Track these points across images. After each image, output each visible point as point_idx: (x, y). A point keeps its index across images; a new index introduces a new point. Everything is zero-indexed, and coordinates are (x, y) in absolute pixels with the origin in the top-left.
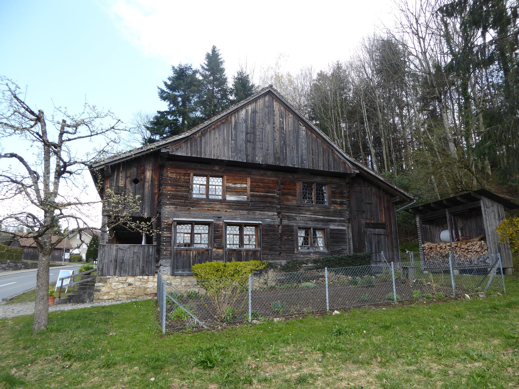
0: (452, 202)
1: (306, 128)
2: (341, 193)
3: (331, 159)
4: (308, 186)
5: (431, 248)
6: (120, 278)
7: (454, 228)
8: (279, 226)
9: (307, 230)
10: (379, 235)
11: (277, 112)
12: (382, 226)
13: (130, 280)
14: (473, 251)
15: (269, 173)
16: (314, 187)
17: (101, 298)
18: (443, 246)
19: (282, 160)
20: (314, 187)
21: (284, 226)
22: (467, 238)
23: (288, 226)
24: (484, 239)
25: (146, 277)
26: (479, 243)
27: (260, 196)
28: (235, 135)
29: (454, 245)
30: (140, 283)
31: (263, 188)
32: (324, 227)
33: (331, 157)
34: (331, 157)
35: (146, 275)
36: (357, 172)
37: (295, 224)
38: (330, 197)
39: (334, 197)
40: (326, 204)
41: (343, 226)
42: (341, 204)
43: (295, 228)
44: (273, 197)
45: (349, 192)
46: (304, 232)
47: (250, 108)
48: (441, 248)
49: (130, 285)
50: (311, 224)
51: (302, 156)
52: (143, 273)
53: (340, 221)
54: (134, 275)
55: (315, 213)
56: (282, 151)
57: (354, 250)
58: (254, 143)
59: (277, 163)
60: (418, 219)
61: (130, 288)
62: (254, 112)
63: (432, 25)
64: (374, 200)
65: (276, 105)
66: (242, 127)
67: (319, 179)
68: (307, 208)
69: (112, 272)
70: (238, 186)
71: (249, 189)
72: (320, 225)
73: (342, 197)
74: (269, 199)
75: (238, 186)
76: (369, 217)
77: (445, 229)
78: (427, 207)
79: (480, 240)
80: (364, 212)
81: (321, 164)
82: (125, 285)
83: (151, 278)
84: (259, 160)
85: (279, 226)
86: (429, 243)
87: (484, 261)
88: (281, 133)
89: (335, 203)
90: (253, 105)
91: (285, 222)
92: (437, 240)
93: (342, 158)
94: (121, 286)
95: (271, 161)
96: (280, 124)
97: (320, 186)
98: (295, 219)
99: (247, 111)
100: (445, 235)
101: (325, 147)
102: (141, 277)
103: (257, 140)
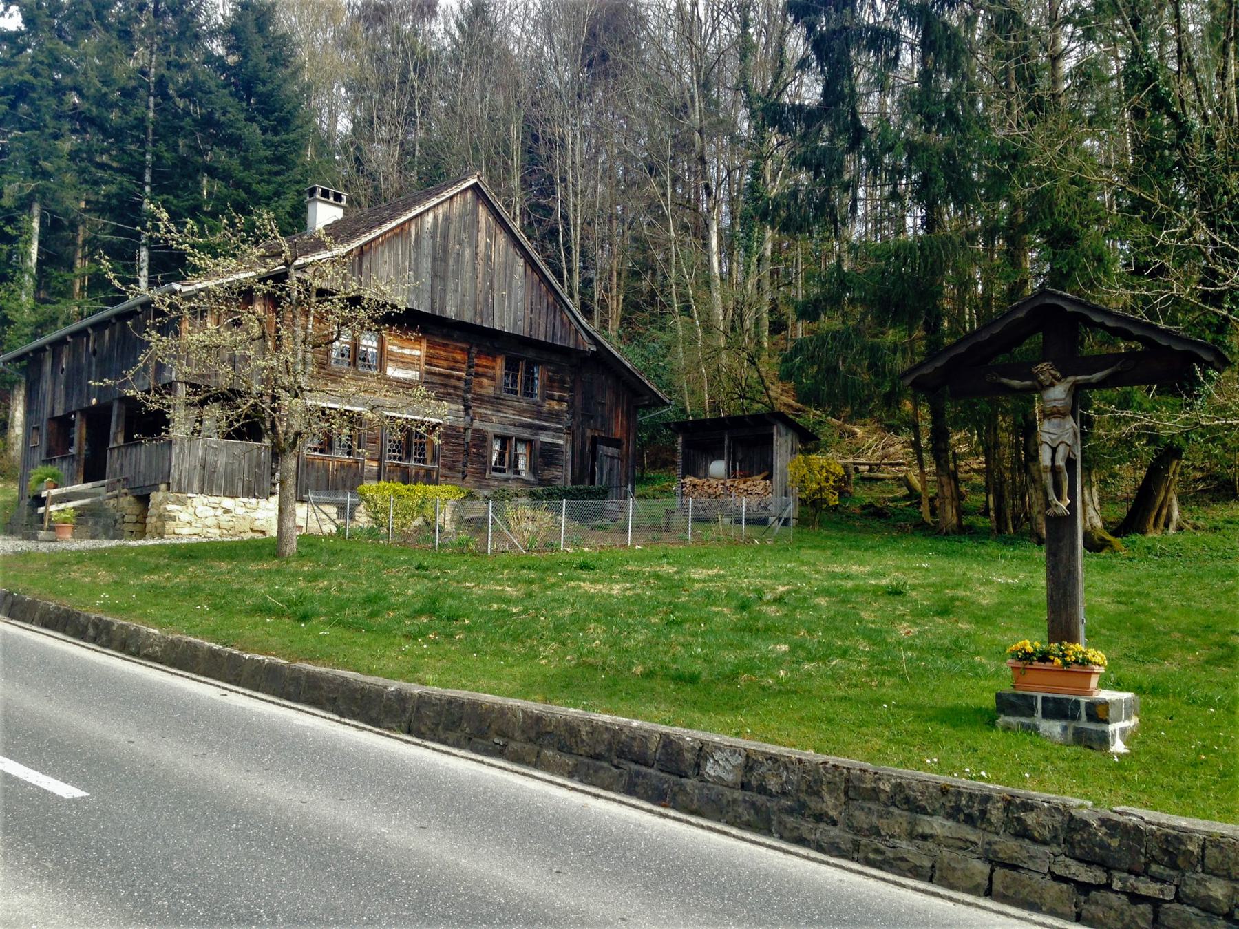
0: (735, 422)
1: (526, 261)
2: (562, 381)
3: (558, 322)
4: (511, 366)
5: (694, 486)
6: (211, 499)
7: (732, 460)
8: (466, 429)
9: (504, 440)
10: (613, 458)
11: (482, 225)
12: (616, 443)
13: (227, 502)
14: (750, 495)
15: (456, 334)
16: (522, 366)
17: (177, 531)
18: (714, 483)
19: (485, 316)
20: (522, 366)
21: (476, 431)
22: (747, 474)
23: (479, 431)
24: (769, 477)
25: (254, 501)
26: (763, 483)
27: (441, 375)
28: (416, 259)
29: (729, 482)
30: (244, 510)
31: (447, 360)
32: (532, 437)
33: (558, 318)
34: (558, 318)
35: (255, 497)
36: (594, 348)
37: (489, 429)
38: (543, 388)
39: (551, 388)
40: (537, 398)
41: (560, 438)
42: (561, 400)
43: (490, 436)
44: (459, 379)
45: (572, 381)
46: (499, 443)
47: (440, 211)
48: (710, 486)
49: (227, 511)
50: (514, 432)
51: (515, 314)
52: (250, 492)
53: (556, 430)
54: (233, 496)
55: (521, 412)
56: (486, 300)
57: (573, 482)
58: (444, 279)
59: (478, 322)
60: (680, 440)
61: (227, 517)
62: (447, 219)
63: (877, 743)
64: (609, 398)
65: (482, 212)
66: (427, 245)
67: (530, 354)
68: (510, 403)
69: (196, 485)
70: (407, 351)
71: (423, 360)
72: (526, 434)
73: (562, 389)
74: (454, 382)
75: (407, 351)
76: (599, 427)
77: (720, 458)
78: (699, 424)
79: (765, 479)
80: (592, 417)
81: (542, 329)
82: (219, 512)
83: (262, 502)
84: (450, 312)
85: (466, 429)
86: (692, 478)
87: (766, 508)
88: (486, 264)
89: (551, 397)
90: (446, 205)
91: (477, 424)
92: (702, 474)
93: (575, 323)
94: (212, 512)
95: (468, 317)
96: (486, 249)
97: (530, 366)
98: (490, 420)
99: (436, 218)
100: (718, 467)
101: (551, 300)
102: (245, 500)
103: (450, 274)
